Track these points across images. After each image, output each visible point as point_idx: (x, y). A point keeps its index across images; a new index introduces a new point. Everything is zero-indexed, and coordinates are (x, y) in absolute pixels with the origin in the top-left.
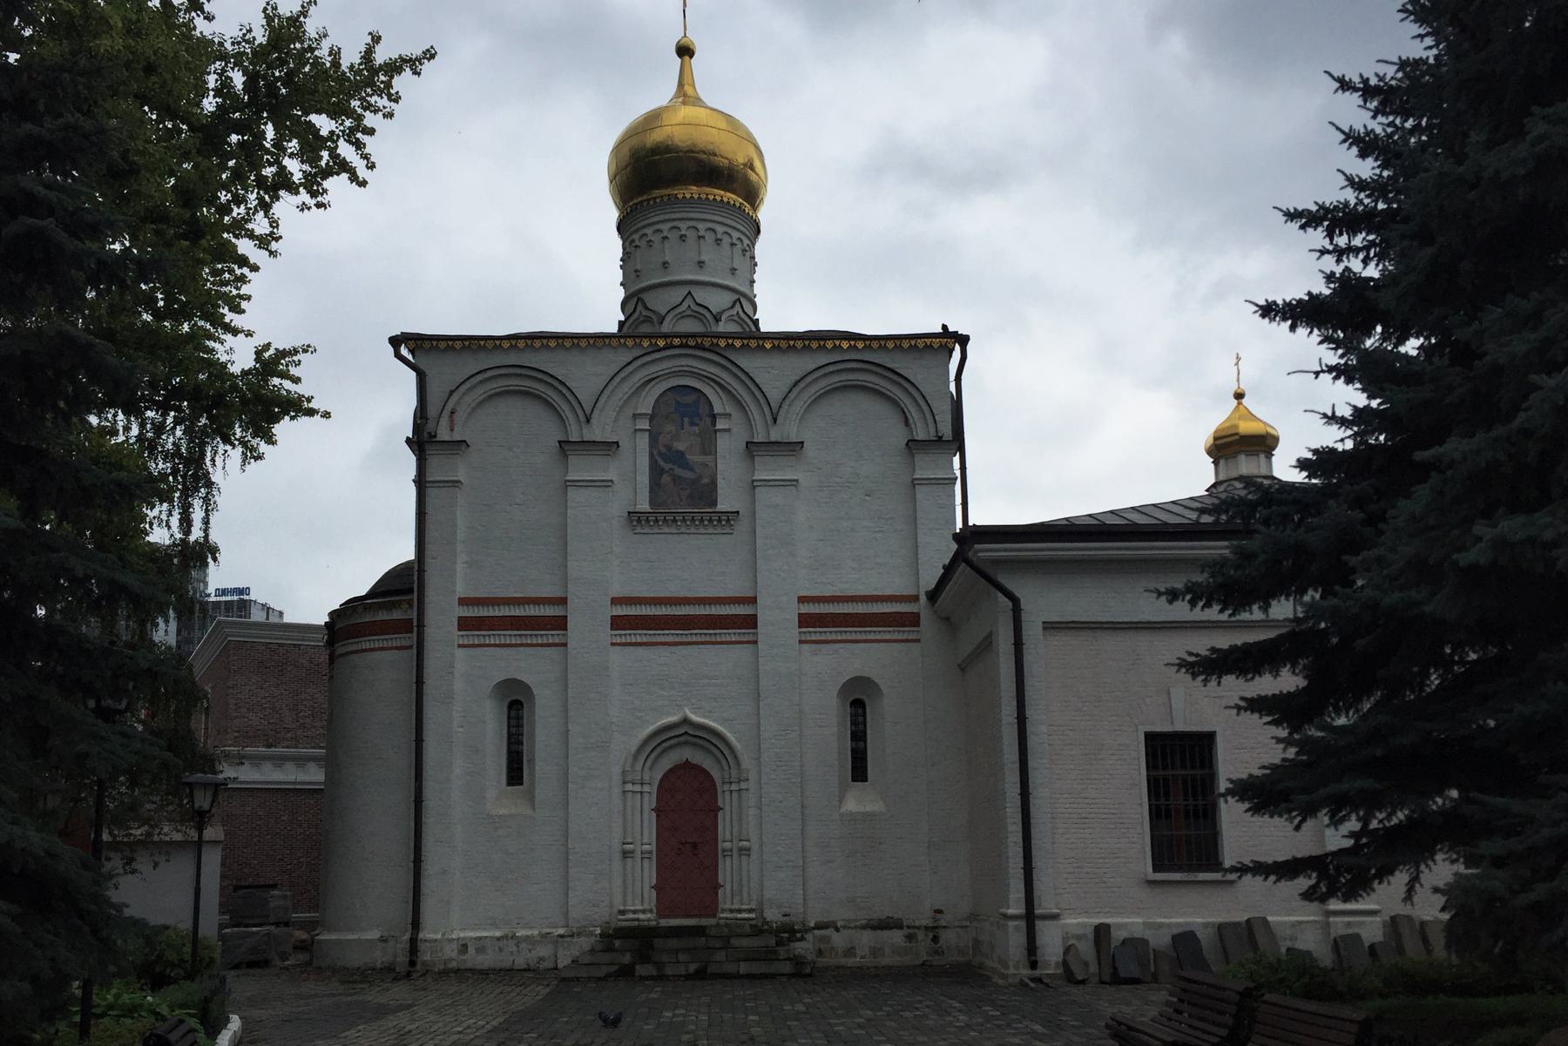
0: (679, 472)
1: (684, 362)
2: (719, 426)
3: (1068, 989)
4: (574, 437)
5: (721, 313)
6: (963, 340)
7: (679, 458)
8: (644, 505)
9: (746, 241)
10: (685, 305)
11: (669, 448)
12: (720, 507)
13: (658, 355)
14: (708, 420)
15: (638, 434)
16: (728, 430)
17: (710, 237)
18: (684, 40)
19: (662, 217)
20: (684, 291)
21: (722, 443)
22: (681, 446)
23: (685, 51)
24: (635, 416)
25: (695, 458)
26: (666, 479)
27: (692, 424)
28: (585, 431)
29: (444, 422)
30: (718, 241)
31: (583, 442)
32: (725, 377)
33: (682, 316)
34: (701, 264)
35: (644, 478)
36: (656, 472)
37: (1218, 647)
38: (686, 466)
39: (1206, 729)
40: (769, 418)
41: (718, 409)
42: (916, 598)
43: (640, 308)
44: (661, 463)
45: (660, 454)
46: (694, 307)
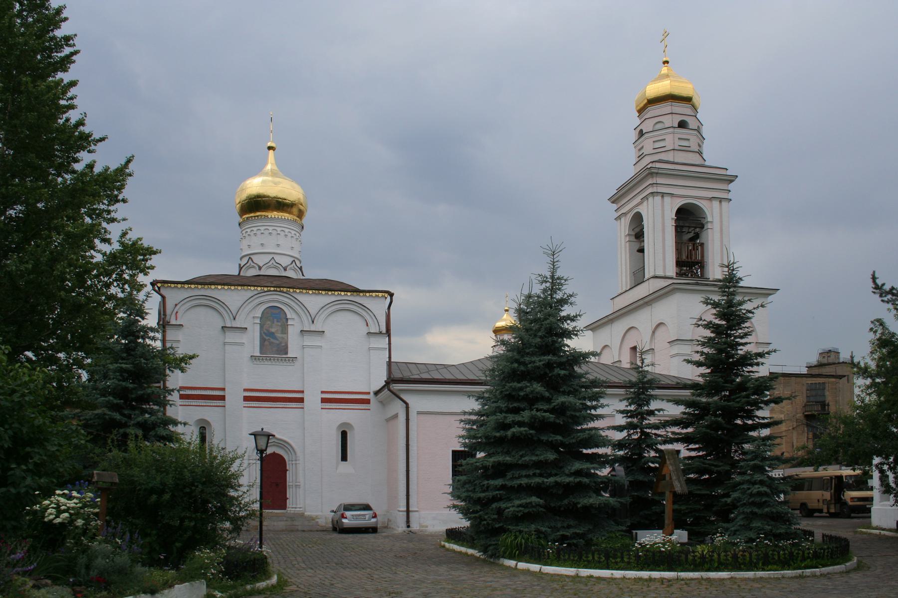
0: (272, 340)
2: (289, 323)
4: (229, 325)
6: (391, 295)
7: (272, 335)
11: (268, 331)
12: (289, 355)
14: (284, 320)
20: (271, 256)
21: (290, 329)
22: (273, 330)
25: (279, 335)
26: (266, 343)
36: (263, 341)
38: (275, 338)
42: (369, 393)
43: (250, 261)
44: (265, 337)
46: (275, 264)
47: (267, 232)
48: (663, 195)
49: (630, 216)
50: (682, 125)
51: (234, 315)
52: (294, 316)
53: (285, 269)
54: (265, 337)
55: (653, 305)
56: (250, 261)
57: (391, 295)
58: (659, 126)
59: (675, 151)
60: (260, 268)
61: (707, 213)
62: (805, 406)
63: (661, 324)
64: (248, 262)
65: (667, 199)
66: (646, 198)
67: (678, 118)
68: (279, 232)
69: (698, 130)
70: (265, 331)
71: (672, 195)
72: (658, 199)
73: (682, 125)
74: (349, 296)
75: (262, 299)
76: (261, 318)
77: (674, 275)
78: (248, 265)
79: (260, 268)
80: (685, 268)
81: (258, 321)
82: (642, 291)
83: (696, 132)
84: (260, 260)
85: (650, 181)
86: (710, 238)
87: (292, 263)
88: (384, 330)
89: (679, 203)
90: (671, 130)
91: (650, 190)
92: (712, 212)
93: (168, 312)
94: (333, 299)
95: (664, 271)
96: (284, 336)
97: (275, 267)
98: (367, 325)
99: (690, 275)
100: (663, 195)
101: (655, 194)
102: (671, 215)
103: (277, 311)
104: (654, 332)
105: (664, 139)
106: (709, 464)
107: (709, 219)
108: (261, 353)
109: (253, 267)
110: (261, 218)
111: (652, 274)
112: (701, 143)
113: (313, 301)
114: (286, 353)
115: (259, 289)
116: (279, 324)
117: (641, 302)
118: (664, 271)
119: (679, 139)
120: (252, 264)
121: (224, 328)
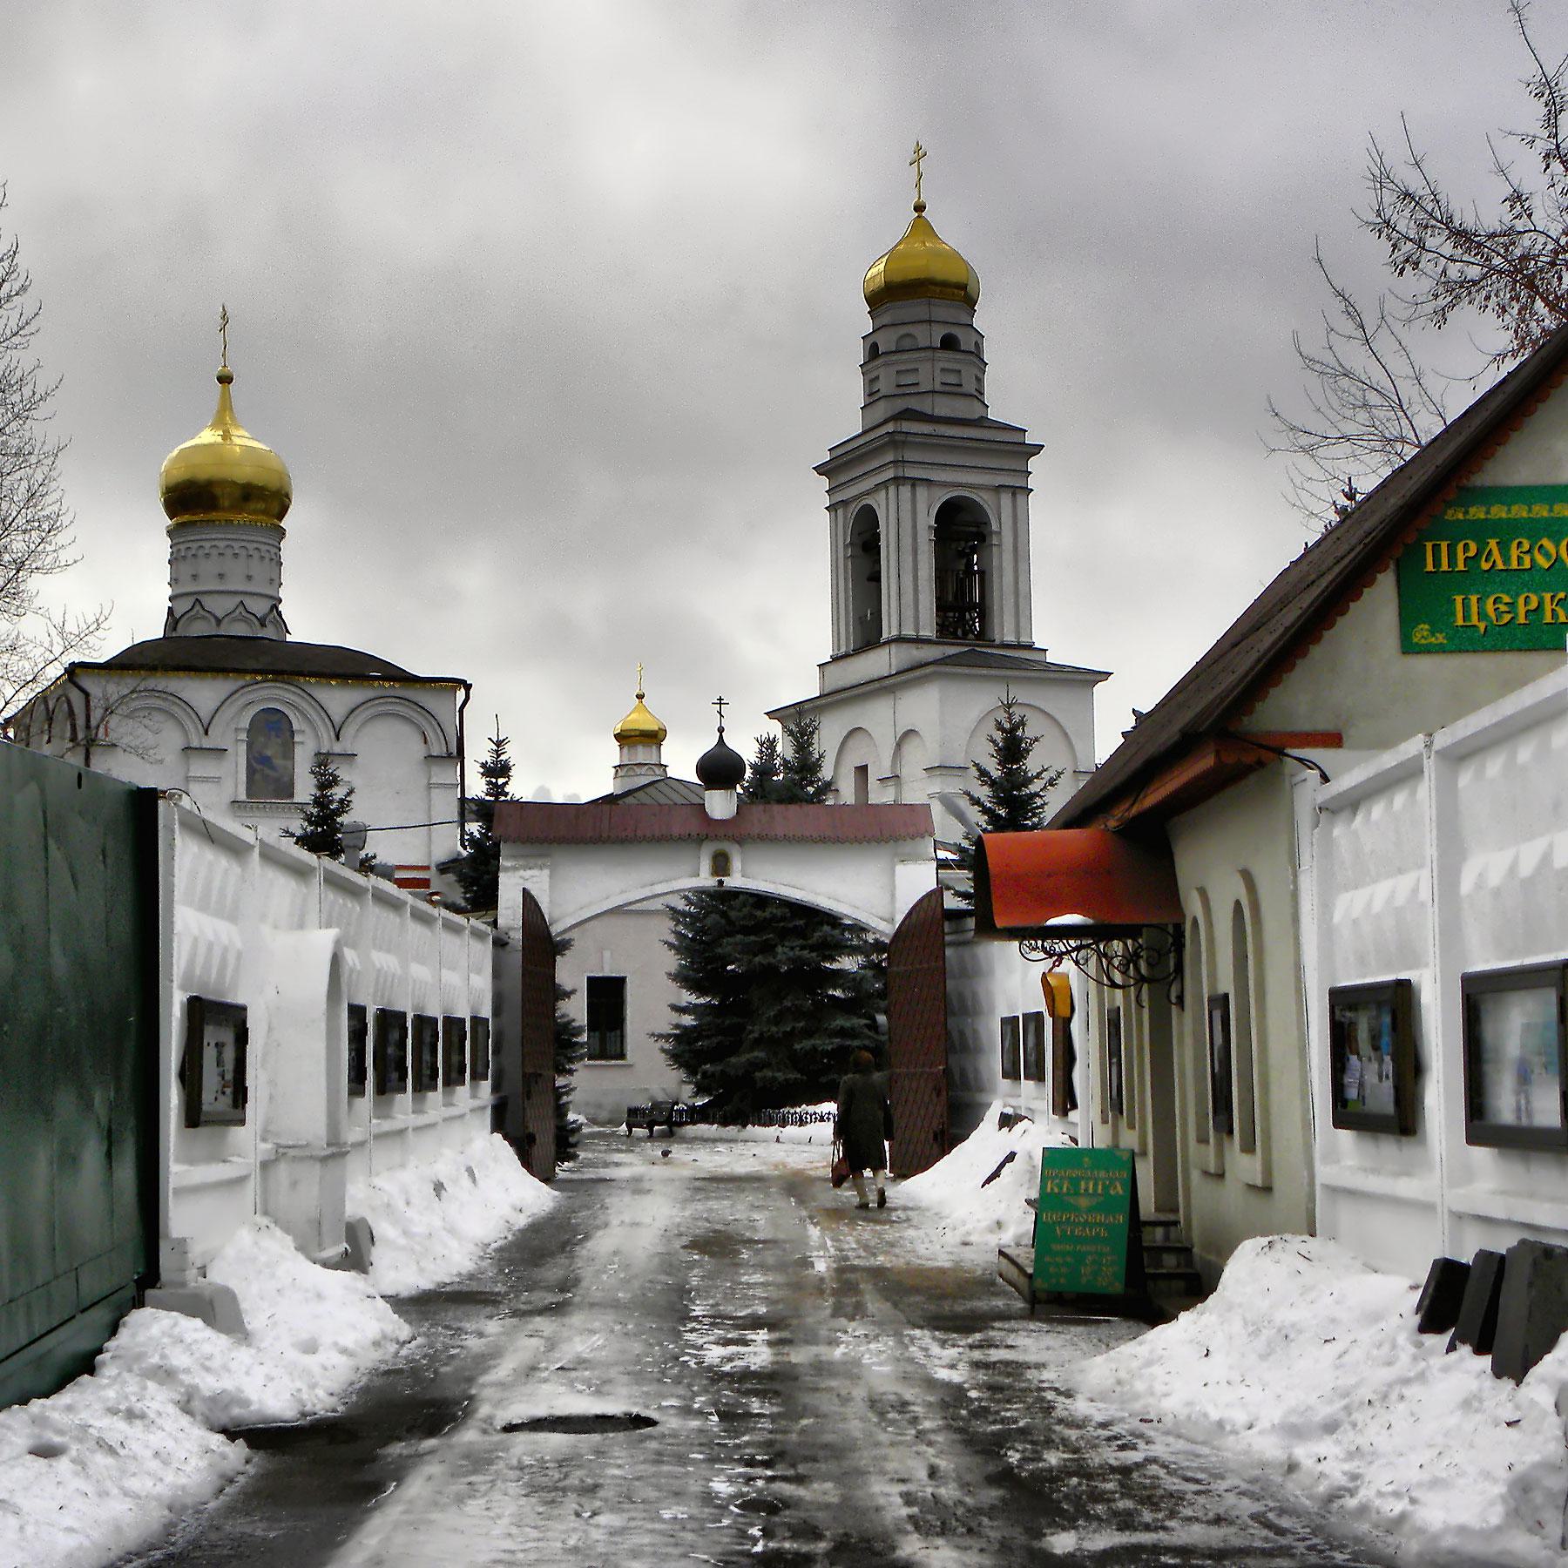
0: (268, 772)
1: (277, 691)
2: (296, 739)
3: (531, 1327)
4: (195, 744)
5: (266, 616)
6: (468, 687)
7: (266, 761)
8: (243, 797)
9: (274, 550)
10: (237, 612)
11: (260, 754)
12: (296, 800)
13: (256, 687)
14: (288, 734)
15: (239, 743)
16: (302, 743)
17: (256, 555)
18: (925, 1559)
19: (220, 536)
20: (238, 599)
21: (298, 751)
22: (269, 753)
23: (225, 380)
24: (237, 730)
25: (278, 762)
26: (257, 777)
27: (277, 736)
28: (203, 741)
29: (101, 730)
30: (262, 558)
31: (202, 749)
32: (304, 705)
33: (235, 620)
34: (249, 578)
35: (243, 777)
36: (251, 772)
37: (221, 1164)
38: (273, 768)
39: (622, 975)
40: (333, 736)
41: (295, 727)
42: (427, 868)
43: (198, 607)
44: (255, 764)
45: (254, 758)
46: (244, 613)
47: (229, 552)
48: (914, 482)
49: (854, 508)
50: (949, 343)
51: (206, 722)
52: (304, 727)
53: (263, 625)
54: (255, 764)
55: (898, 694)
56: (198, 607)
57: (468, 687)
58: (907, 344)
59: (936, 395)
60: (219, 622)
61: (989, 512)
62: (873, 352)
63: (910, 733)
64: (193, 607)
65: (922, 492)
66: (884, 485)
67: (938, 333)
68: (251, 553)
69: (977, 353)
70: (257, 755)
71: (928, 482)
72: (906, 491)
73: (949, 343)
74: (398, 689)
75: (251, 697)
76: (249, 731)
77: (928, 631)
78: (192, 613)
79: (219, 622)
80: (951, 614)
81: (244, 736)
82: (877, 663)
83: (973, 358)
84: (220, 606)
85: (890, 457)
86: (995, 563)
87: (271, 610)
88: (454, 751)
89: (944, 496)
90: (929, 354)
91: (890, 474)
92: (999, 514)
93: (93, 723)
94: (370, 694)
95: (917, 630)
96: (289, 763)
97: (245, 620)
98: (426, 742)
99: (960, 632)
100: (914, 482)
101: (901, 481)
102: (927, 520)
103: (278, 716)
104: (899, 745)
105: (917, 370)
106: (742, 1524)
107: (994, 527)
108: (248, 798)
109: (203, 618)
110: (220, 525)
111: (895, 632)
112: (980, 375)
113: (338, 699)
114: (292, 796)
115: (248, 678)
116: (279, 741)
117: (877, 685)
118: (917, 630)
119: (943, 370)
120: (202, 612)
121: (187, 749)
